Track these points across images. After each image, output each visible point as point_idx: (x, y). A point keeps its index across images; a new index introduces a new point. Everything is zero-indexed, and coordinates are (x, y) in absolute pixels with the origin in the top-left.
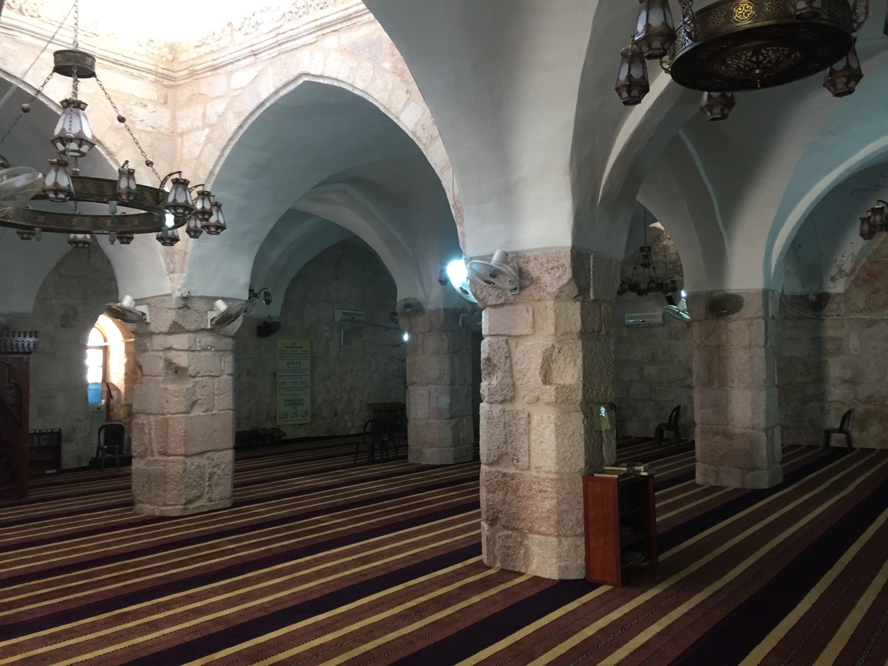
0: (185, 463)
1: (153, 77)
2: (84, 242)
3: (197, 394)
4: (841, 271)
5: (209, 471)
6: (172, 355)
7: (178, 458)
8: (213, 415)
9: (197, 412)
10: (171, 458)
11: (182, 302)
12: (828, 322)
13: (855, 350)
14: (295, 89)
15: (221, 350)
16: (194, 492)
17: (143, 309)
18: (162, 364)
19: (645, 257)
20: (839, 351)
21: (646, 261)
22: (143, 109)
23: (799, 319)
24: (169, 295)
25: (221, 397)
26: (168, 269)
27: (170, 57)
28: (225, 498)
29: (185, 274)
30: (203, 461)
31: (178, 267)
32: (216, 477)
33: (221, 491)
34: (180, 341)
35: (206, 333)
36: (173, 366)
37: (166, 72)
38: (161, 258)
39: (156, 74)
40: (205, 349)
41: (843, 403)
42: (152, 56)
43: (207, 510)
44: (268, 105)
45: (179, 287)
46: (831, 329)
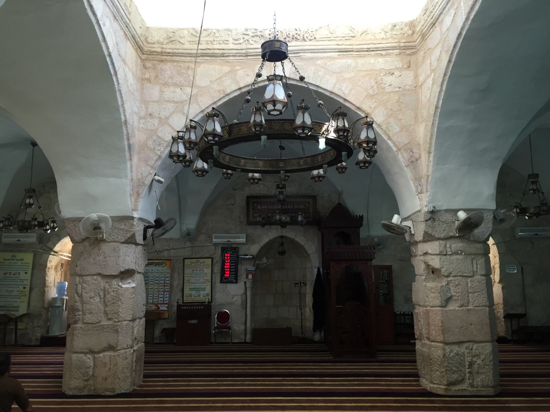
0: (445, 350)
1: (397, 51)
2: (319, 176)
3: (452, 291)
5: (469, 359)
6: (428, 258)
7: (438, 344)
8: (468, 310)
9: (453, 306)
10: (433, 343)
11: (429, 216)
14: (480, 7)
15: (471, 254)
16: (455, 376)
17: (408, 223)
18: (423, 266)
22: (391, 77)
24: (419, 211)
25: (476, 294)
26: (417, 191)
27: (410, 32)
28: (488, 386)
29: (429, 193)
30: (463, 349)
31: (425, 190)
32: (476, 366)
33: (484, 379)
34: (433, 247)
35: (457, 240)
37: (407, 44)
38: (411, 182)
39: (400, 48)
40: (456, 253)
42: (395, 36)
43: (468, 394)
44: (464, 33)
45: (425, 203)
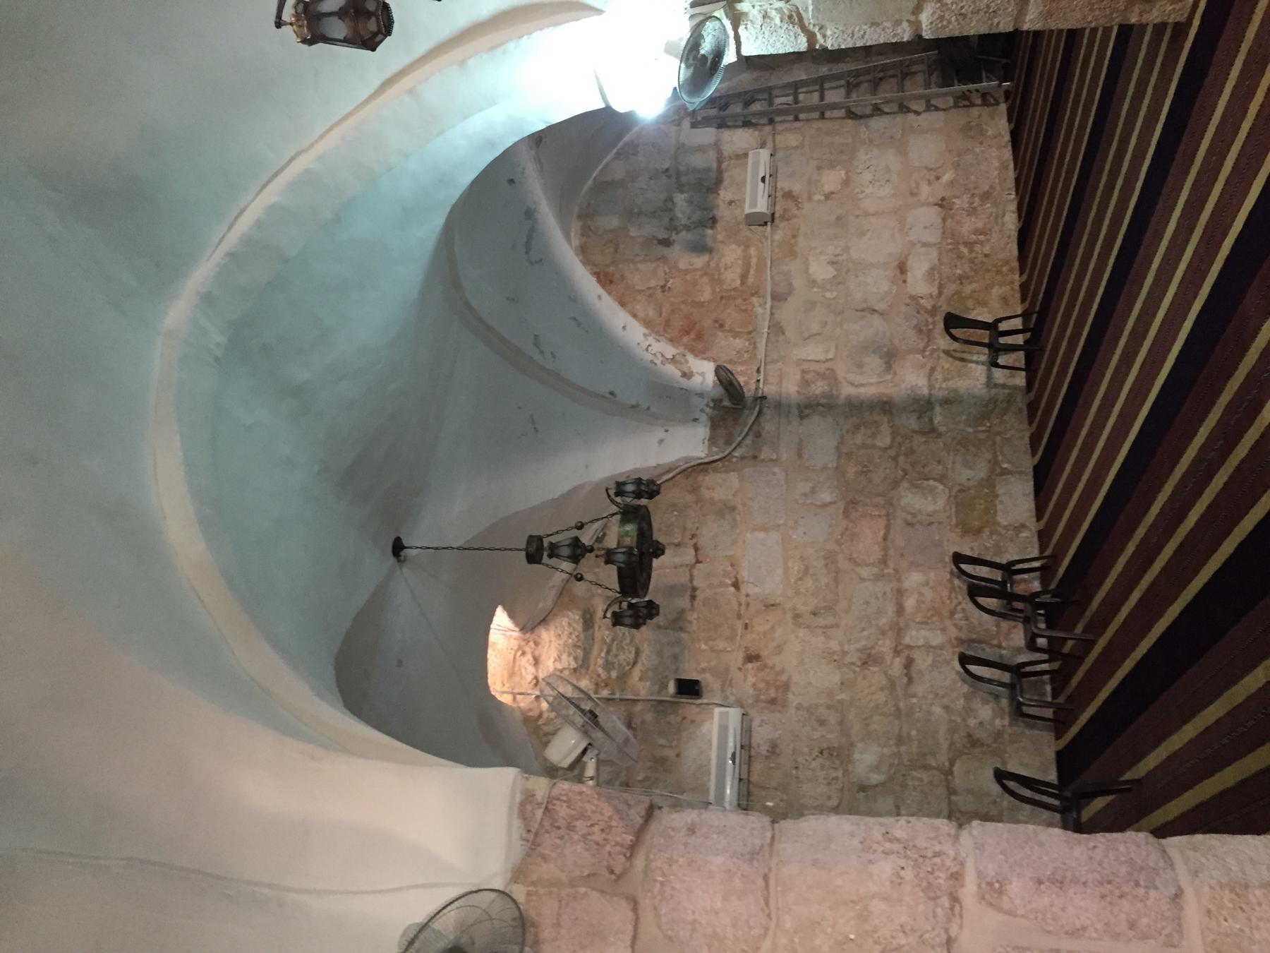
4: (673, 360)
12: (769, 390)
13: (827, 352)
19: (554, 551)
20: (831, 377)
21: (565, 551)
23: (758, 435)
36: (815, 787)
41: (933, 369)
46: (785, 383)
